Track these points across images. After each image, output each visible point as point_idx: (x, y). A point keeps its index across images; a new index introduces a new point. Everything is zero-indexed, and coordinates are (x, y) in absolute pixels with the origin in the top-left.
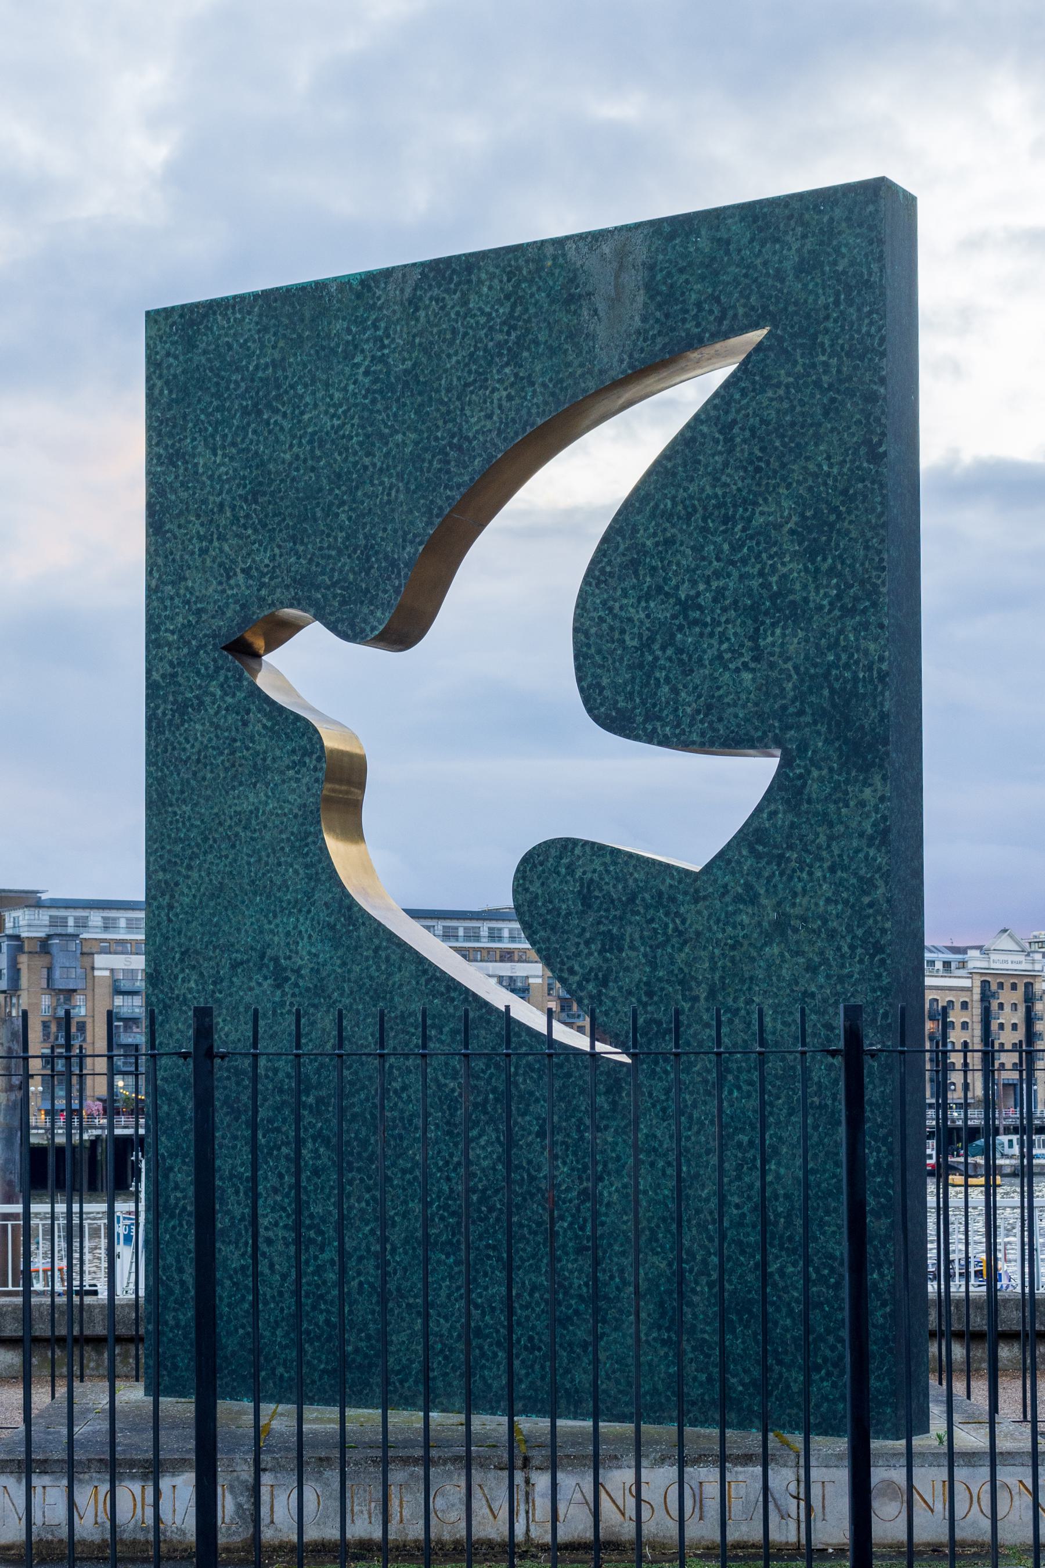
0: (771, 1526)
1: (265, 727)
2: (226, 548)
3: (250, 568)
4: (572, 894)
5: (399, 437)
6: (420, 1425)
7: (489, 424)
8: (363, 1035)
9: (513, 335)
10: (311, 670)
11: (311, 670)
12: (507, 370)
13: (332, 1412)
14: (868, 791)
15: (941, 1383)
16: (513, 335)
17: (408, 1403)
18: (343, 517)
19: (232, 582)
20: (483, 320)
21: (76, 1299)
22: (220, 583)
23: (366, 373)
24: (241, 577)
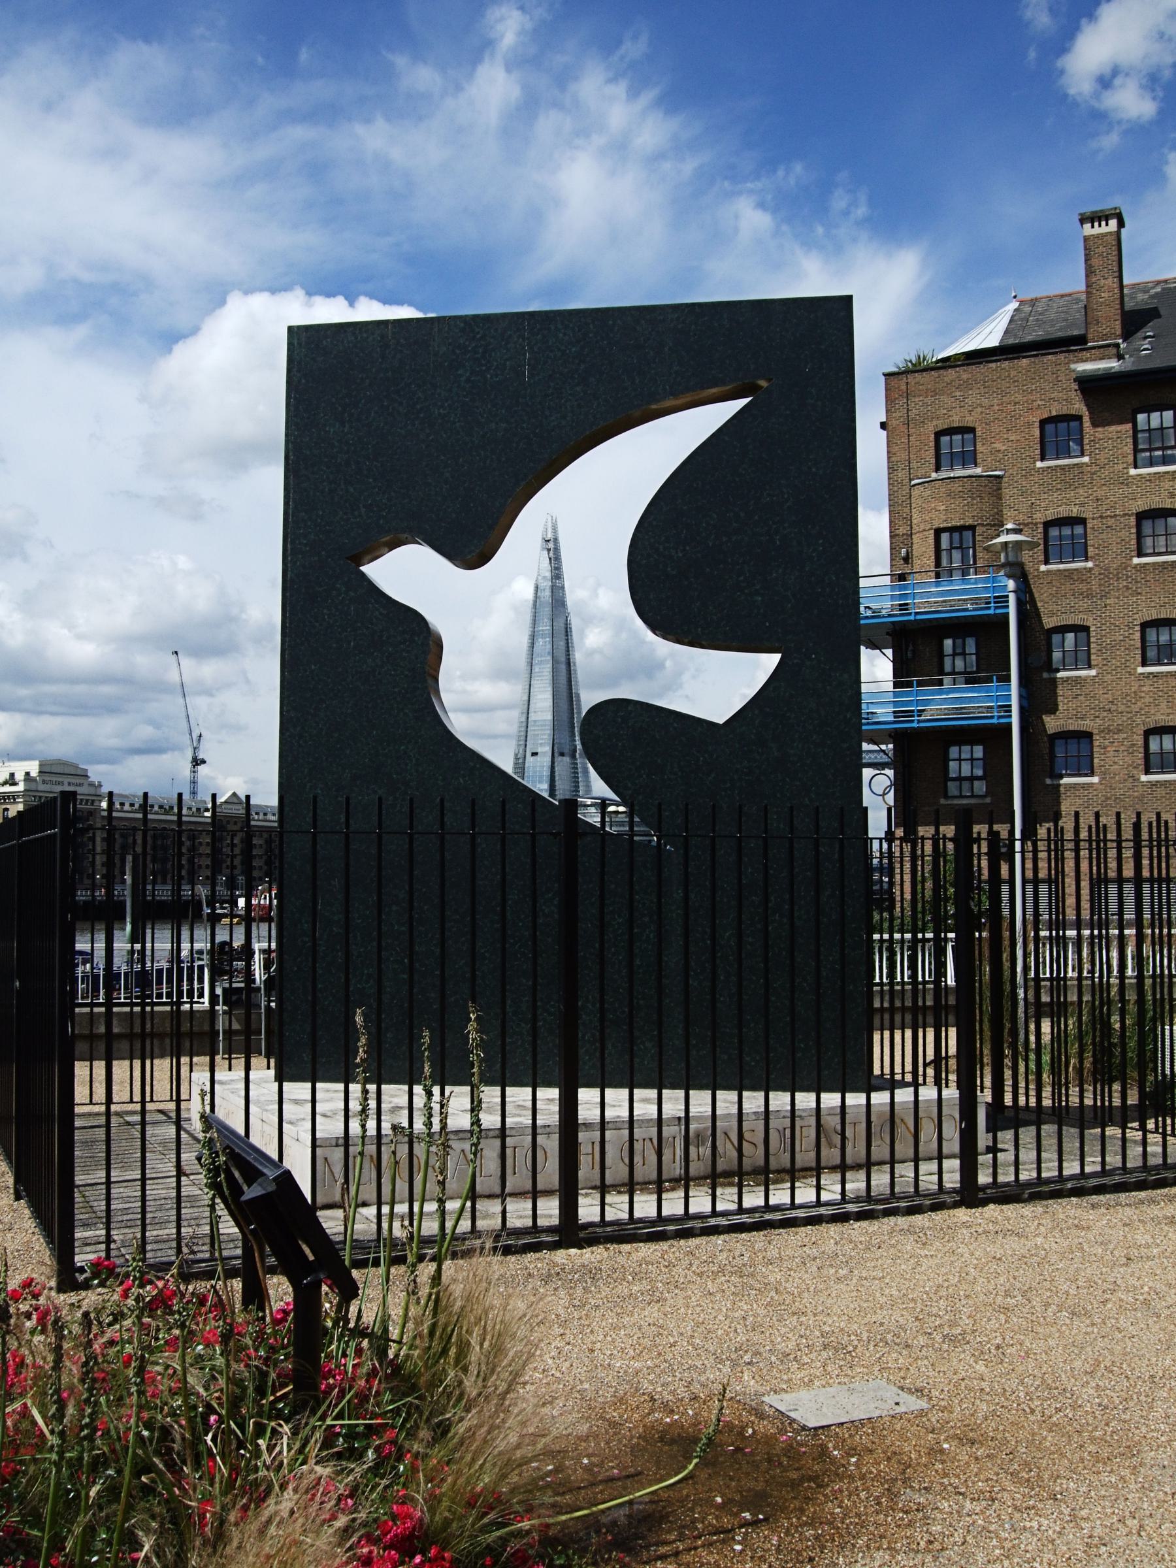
0: (318, 1168)
1: (381, 614)
2: (352, 490)
3: (371, 505)
4: (622, 734)
5: (493, 426)
6: (814, 1105)
7: (564, 423)
8: (1108, 820)
9: (582, 366)
10: (408, 573)
11: (408, 573)
12: (578, 389)
13: (786, 1097)
14: (846, 676)
15: (268, 1068)
16: (582, 366)
17: (806, 1089)
18: (448, 475)
19: (356, 513)
20: (559, 354)
21: (148, 1009)
22: (346, 514)
23: (468, 380)
24: (363, 510)
